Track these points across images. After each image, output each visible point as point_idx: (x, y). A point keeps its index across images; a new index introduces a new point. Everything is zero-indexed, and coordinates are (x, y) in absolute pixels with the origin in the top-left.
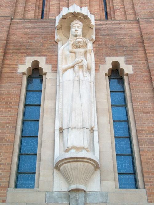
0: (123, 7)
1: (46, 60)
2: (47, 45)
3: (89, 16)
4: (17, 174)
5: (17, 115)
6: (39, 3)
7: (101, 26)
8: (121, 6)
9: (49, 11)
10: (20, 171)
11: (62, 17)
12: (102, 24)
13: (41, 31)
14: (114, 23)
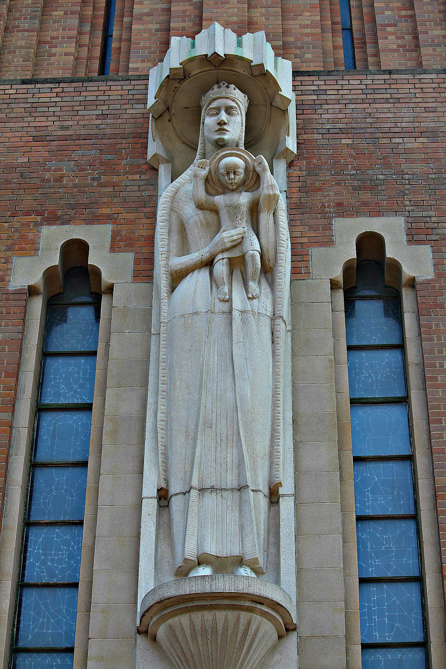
0: (409, 13)
1: (115, 235)
2: (115, 179)
3: (269, 67)
4: (11, 655)
5: (9, 446)
6: (94, 9)
7: (323, 97)
8: (403, 13)
9: (129, 40)
10: (21, 644)
11: (167, 73)
12: (324, 87)
13: (98, 122)
14: (369, 82)
